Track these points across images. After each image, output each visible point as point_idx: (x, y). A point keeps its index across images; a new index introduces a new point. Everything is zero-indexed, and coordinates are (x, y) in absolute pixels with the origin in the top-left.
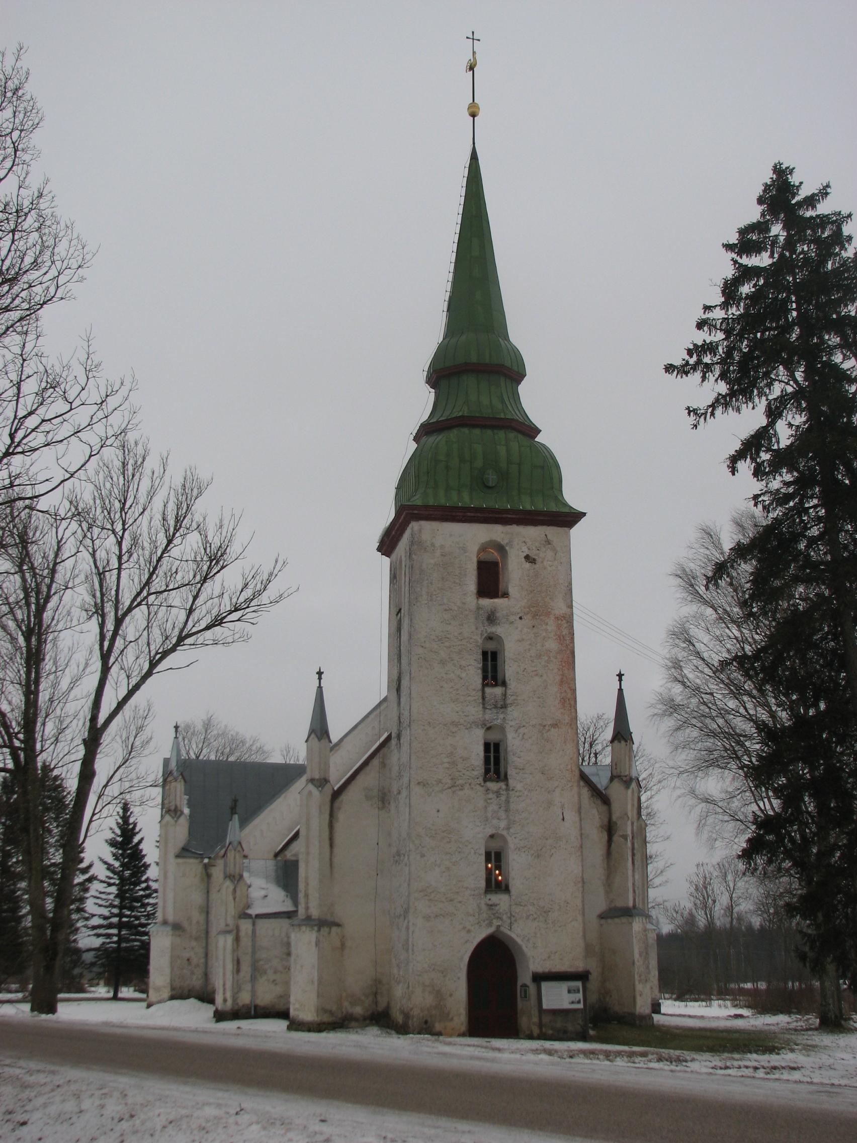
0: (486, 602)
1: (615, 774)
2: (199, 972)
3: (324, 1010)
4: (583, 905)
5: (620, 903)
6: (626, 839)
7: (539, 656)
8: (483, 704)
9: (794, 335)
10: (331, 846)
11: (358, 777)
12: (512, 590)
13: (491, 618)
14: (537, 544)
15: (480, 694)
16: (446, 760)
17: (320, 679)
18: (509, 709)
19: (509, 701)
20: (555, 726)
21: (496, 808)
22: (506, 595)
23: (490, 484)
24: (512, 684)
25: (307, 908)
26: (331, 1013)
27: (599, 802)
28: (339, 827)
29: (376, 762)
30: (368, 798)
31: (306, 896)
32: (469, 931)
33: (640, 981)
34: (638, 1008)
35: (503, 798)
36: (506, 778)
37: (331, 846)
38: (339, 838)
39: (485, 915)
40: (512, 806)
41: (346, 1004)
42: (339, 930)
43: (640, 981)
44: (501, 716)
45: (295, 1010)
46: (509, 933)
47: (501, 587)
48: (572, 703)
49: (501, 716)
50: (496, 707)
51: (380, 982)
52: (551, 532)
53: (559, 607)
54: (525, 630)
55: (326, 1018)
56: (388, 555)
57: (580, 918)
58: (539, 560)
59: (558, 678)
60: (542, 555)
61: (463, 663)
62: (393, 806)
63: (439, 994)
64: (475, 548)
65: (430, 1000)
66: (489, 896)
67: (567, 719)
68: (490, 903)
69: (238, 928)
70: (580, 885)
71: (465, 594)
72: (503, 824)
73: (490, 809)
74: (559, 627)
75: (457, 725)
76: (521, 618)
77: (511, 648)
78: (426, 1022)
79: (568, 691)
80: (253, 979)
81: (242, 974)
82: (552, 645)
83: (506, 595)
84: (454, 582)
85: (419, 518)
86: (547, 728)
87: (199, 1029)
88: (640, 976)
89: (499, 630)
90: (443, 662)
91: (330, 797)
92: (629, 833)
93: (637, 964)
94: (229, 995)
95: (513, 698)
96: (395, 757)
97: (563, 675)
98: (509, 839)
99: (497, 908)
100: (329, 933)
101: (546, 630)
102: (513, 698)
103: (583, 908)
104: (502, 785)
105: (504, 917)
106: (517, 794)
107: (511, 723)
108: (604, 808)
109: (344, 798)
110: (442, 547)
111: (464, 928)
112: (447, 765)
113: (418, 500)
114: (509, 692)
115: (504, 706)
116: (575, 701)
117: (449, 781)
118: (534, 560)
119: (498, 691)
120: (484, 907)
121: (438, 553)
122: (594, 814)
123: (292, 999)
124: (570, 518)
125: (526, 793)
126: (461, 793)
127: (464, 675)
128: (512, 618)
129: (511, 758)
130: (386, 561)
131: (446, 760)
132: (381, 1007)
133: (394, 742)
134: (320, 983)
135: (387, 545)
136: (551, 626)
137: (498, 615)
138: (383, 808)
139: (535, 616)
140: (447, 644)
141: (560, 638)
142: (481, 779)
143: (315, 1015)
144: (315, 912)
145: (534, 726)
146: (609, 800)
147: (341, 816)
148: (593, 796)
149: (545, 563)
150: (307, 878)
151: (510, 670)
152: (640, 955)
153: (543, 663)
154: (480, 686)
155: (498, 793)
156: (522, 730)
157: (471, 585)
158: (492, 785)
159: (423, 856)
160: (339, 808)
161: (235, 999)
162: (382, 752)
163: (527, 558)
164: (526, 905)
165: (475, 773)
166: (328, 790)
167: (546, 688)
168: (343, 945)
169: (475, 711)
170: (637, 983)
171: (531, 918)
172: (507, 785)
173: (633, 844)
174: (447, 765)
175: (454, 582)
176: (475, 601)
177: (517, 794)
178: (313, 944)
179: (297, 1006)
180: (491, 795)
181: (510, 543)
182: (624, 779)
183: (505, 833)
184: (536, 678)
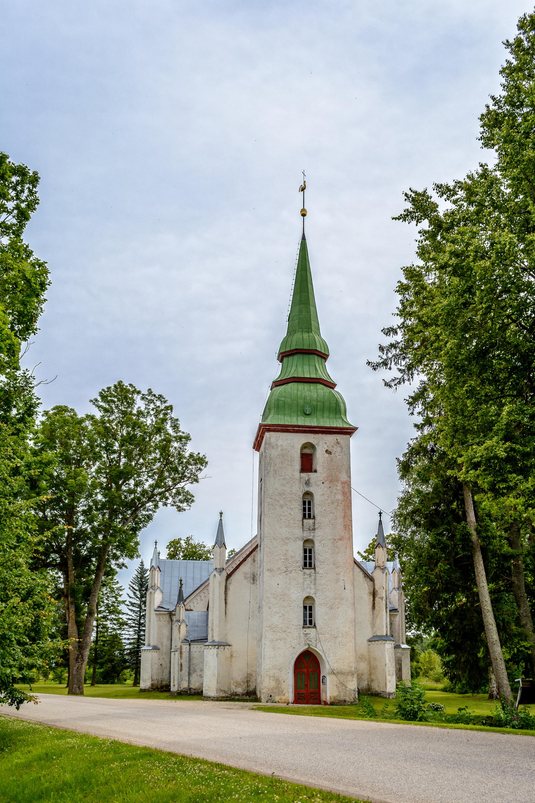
0: (304, 475)
1: (377, 565)
2: (166, 671)
3: (219, 690)
4: (355, 634)
5: (379, 634)
6: (382, 600)
7: (333, 503)
8: (303, 528)
9: (474, 344)
10: (226, 603)
11: (240, 567)
12: (319, 468)
13: (308, 483)
14: (332, 444)
15: (301, 523)
16: (283, 557)
17: (221, 516)
18: (316, 531)
19: (316, 527)
20: (341, 539)
21: (309, 583)
22: (316, 471)
23: (308, 413)
24: (318, 518)
25: (213, 636)
26: (225, 692)
27: (368, 580)
28: (230, 593)
29: (249, 559)
30: (245, 578)
31: (212, 630)
32: (294, 648)
33: (389, 675)
34: (388, 689)
35: (313, 577)
36: (315, 568)
37: (226, 603)
38: (357, 570)
39: (302, 639)
40: (318, 582)
41: (233, 687)
42: (230, 648)
43: (389, 675)
44: (312, 534)
45: (205, 690)
46: (315, 649)
47: (314, 468)
48: (350, 527)
49: (312, 534)
50: (309, 530)
51: (251, 675)
52: (339, 437)
53: (343, 477)
54: (325, 489)
55: (222, 694)
56: (258, 451)
57: (353, 641)
58: (333, 453)
59: (343, 514)
60: (334, 450)
61: (292, 507)
62: (258, 583)
63: (277, 681)
64: (300, 447)
65: (273, 684)
66: (305, 629)
67: (347, 536)
68: (305, 633)
69: (181, 648)
70: (353, 623)
71: (294, 471)
72: (312, 591)
73: (306, 583)
74: (343, 487)
75: (288, 540)
76: (323, 483)
77: (318, 499)
78: (271, 696)
79: (348, 521)
80: (189, 674)
81: (183, 672)
82: (340, 497)
83: (316, 471)
84: (288, 464)
85: (269, 430)
86: (336, 540)
87: (238, 693)
88: (389, 672)
89: (311, 489)
90: (282, 506)
91: (225, 578)
92: (384, 596)
93: (387, 666)
94: (176, 683)
95: (319, 525)
96: (258, 555)
97: (345, 513)
98: (315, 599)
99: (309, 635)
100: (224, 649)
101: (337, 489)
102: (319, 525)
103: (355, 636)
104: (313, 571)
105: (313, 640)
106: (320, 575)
107: (317, 538)
108: (371, 583)
109: (233, 578)
110: (282, 446)
111: (291, 646)
112: (283, 560)
113: (268, 422)
114: (316, 522)
115: (314, 529)
116: (352, 527)
117: (284, 569)
118: (331, 452)
119: (311, 521)
120: (302, 635)
121: (280, 449)
122: (365, 587)
123: (204, 685)
124: (349, 431)
125: (325, 575)
126: (291, 575)
127: (292, 513)
128: (319, 483)
129: (317, 556)
130: (257, 454)
131: (283, 557)
132: (251, 688)
133: (259, 548)
134: (218, 676)
135: (257, 446)
136: (339, 487)
137: (311, 481)
138: (253, 583)
139: (331, 481)
140: (284, 497)
141: (344, 494)
142: (301, 568)
143: (216, 692)
144: (216, 639)
145: (329, 540)
146: (373, 578)
147: (231, 587)
148: (365, 576)
149: (336, 454)
150: (213, 620)
151: (317, 510)
152: (389, 661)
153: (335, 507)
154: (301, 519)
155: (310, 575)
156: (323, 542)
157: (297, 465)
158: (307, 571)
159: (270, 608)
160: (230, 584)
161: (179, 685)
162: (252, 555)
163: (327, 451)
164: (324, 634)
165: (298, 564)
166: (224, 574)
167: (336, 519)
168: (232, 656)
169: (298, 532)
170: (387, 675)
171: (327, 641)
172: (315, 571)
173: (386, 602)
174: (283, 560)
175: (288, 464)
176: (299, 474)
177: (320, 575)
178: (215, 655)
179: (207, 688)
180: (306, 576)
181: (318, 444)
182: (382, 568)
183: (313, 596)
184: (331, 514)
